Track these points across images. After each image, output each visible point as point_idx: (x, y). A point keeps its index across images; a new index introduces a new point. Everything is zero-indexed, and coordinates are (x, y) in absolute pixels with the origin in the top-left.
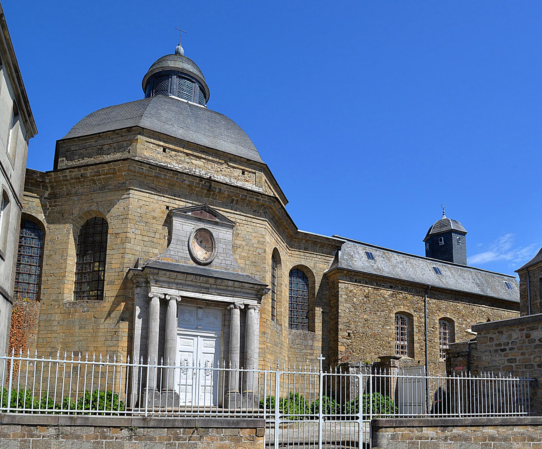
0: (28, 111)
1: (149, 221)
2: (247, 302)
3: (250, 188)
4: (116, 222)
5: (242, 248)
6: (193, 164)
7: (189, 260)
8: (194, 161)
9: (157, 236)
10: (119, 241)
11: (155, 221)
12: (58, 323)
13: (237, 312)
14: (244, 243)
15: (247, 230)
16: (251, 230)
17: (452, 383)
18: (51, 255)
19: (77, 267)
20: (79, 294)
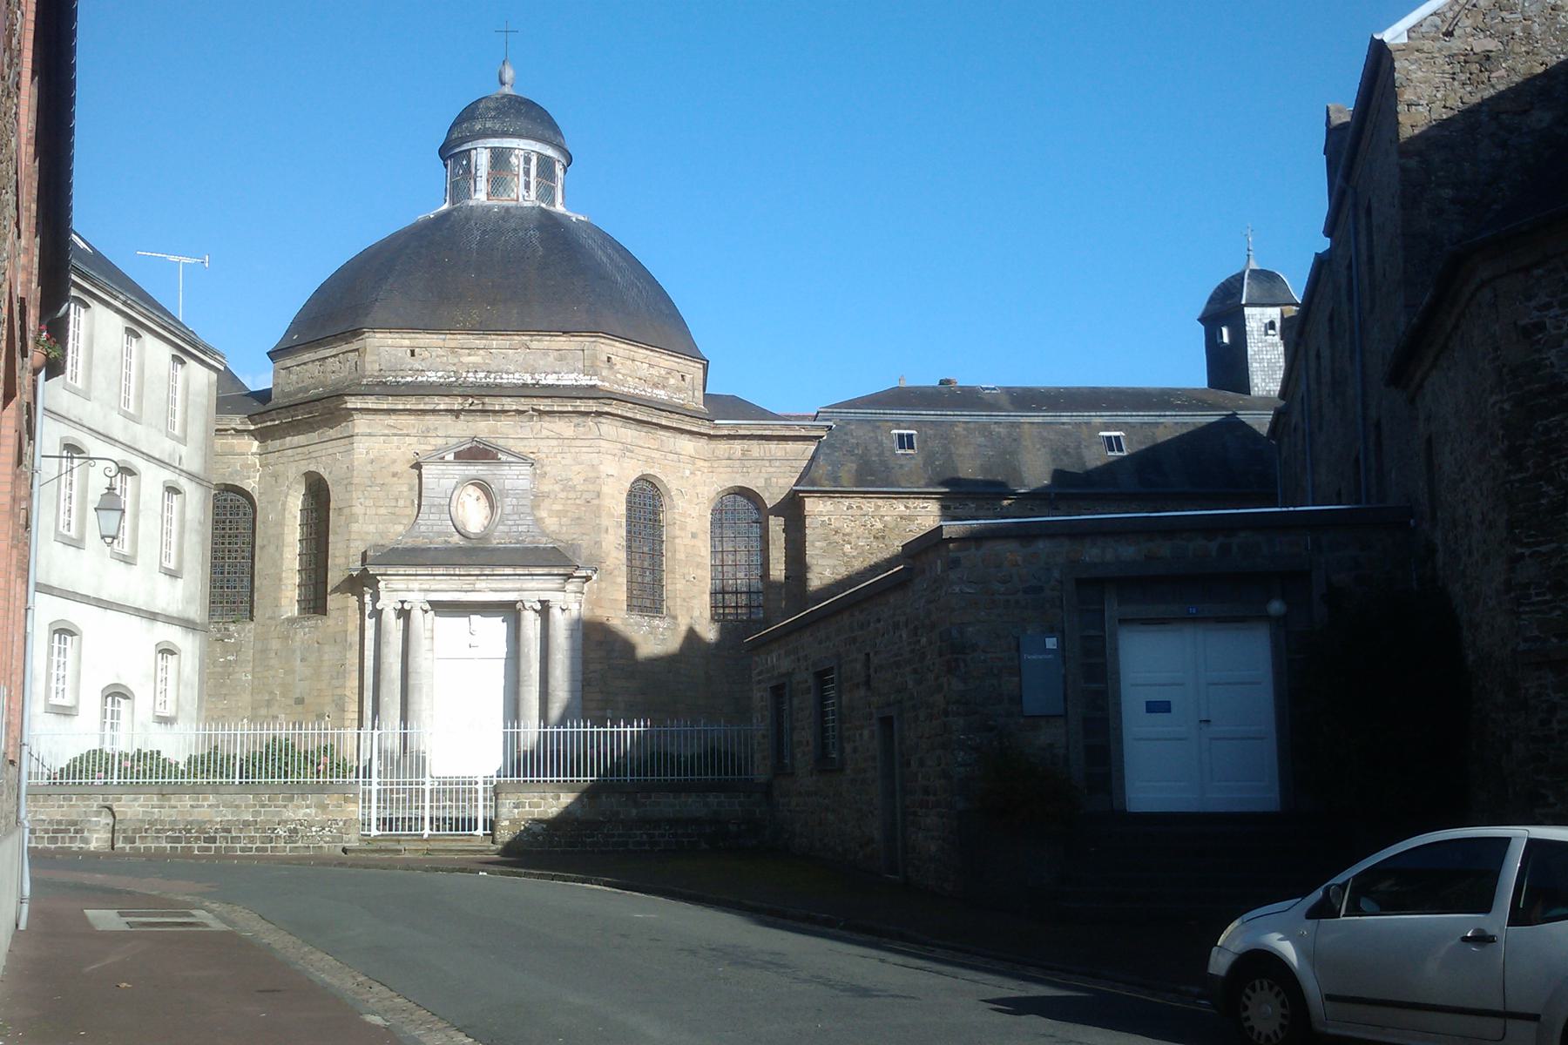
9: (401, 503)
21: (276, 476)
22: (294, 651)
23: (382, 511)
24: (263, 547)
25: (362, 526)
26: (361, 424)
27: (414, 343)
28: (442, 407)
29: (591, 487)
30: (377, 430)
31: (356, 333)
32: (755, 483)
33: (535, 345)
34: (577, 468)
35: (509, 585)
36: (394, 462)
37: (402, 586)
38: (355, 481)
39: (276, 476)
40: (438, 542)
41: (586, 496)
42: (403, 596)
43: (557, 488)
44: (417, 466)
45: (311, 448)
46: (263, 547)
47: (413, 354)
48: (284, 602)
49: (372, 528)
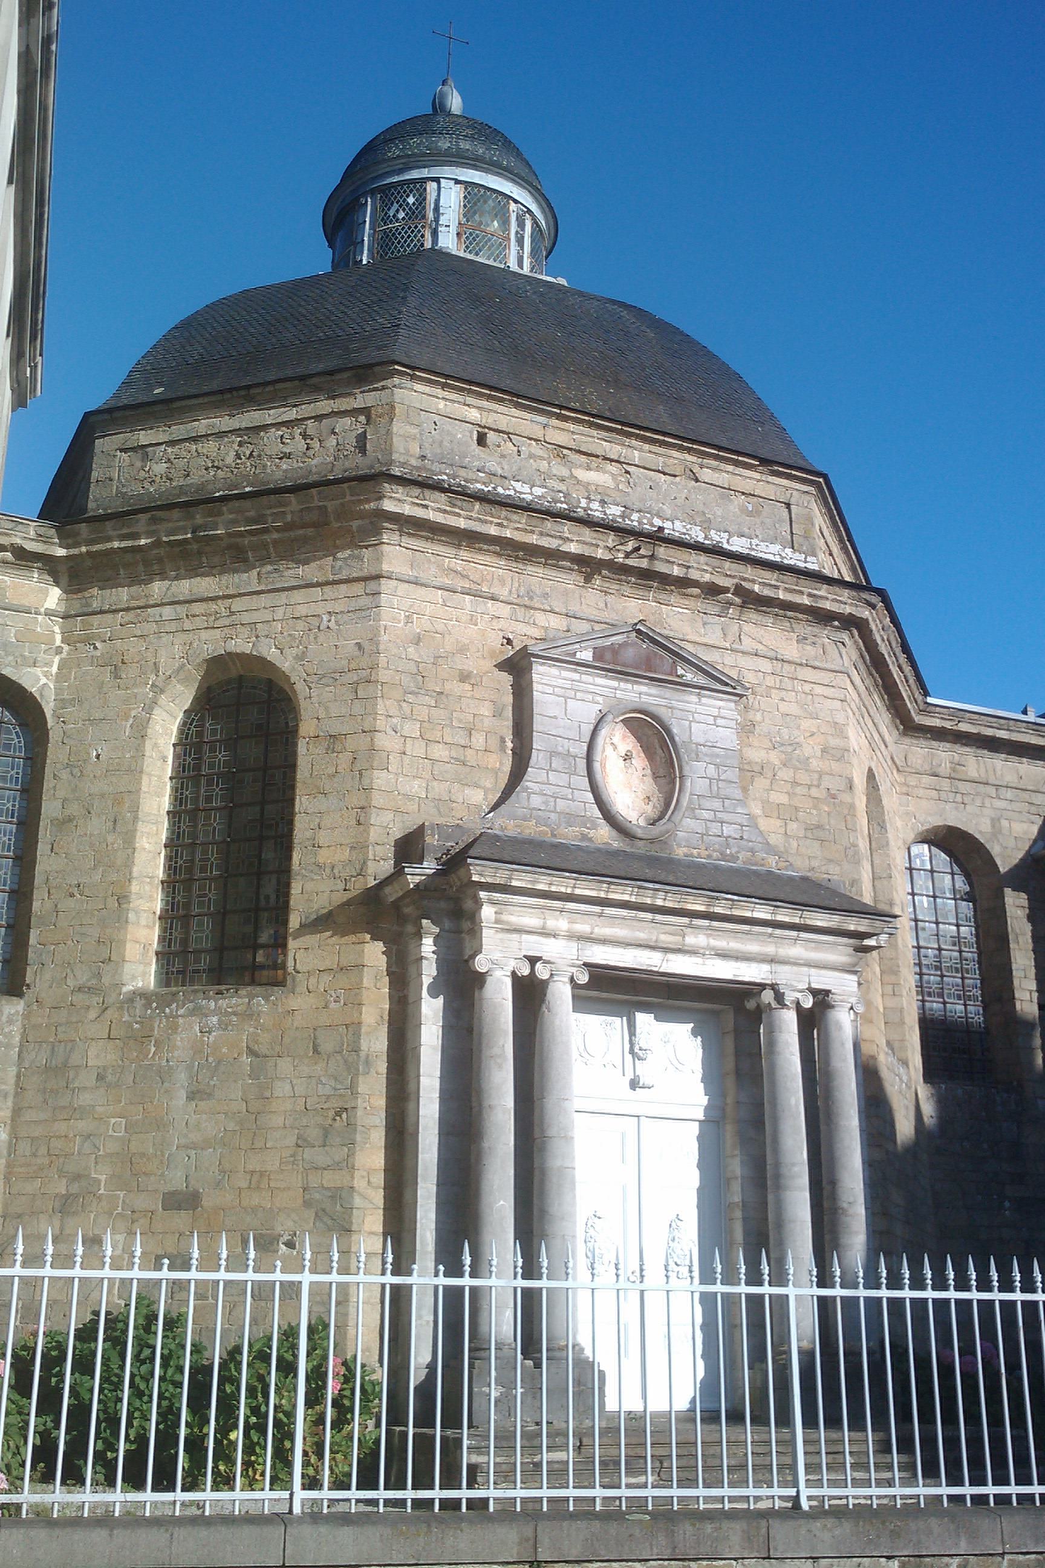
0: (34, 322)
1: (448, 686)
2: (823, 980)
3: (778, 559)
4: (328, 693)
5: (770, 775)
6: (579, 482)
7: (595, 826)
8: (582, 475)
9: (479, 740)
10: (344, 759)
11: (468, 687)
12: (100, 1077)
13: (789, 1020)
14: (774, 758)
15: (784, 707)
16: (793, 709)
17: (977, 1463)
18: (70, 819)
19: (169, 858)
20: (180, 963)
21: (116, 666)
22: (164, 1075)
23: (439, 752)
24: (64, 823)
25: (396, 772)
26: (396, 554)
27: (489, 420)
28: (573, 548)
29: (835, 766)
30: (430, 573)
31: (368, 372)
32: (976, 822)
33: (706, 475)
34: (807, 724)
35: (753, 947)
36: (462, 650)
37: (531, 920)
38: (383, 675)
39: (116, 666)
40: (569, 835)
41: (827, 782)
42: (534, 945)
43: (774, 758)
44: (517, 666)
45: (237, 604)
46: (64, 823)
47: (481, 440)
48: (132, 951)
49: (416, 787)
